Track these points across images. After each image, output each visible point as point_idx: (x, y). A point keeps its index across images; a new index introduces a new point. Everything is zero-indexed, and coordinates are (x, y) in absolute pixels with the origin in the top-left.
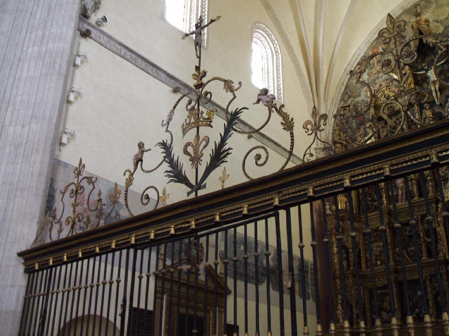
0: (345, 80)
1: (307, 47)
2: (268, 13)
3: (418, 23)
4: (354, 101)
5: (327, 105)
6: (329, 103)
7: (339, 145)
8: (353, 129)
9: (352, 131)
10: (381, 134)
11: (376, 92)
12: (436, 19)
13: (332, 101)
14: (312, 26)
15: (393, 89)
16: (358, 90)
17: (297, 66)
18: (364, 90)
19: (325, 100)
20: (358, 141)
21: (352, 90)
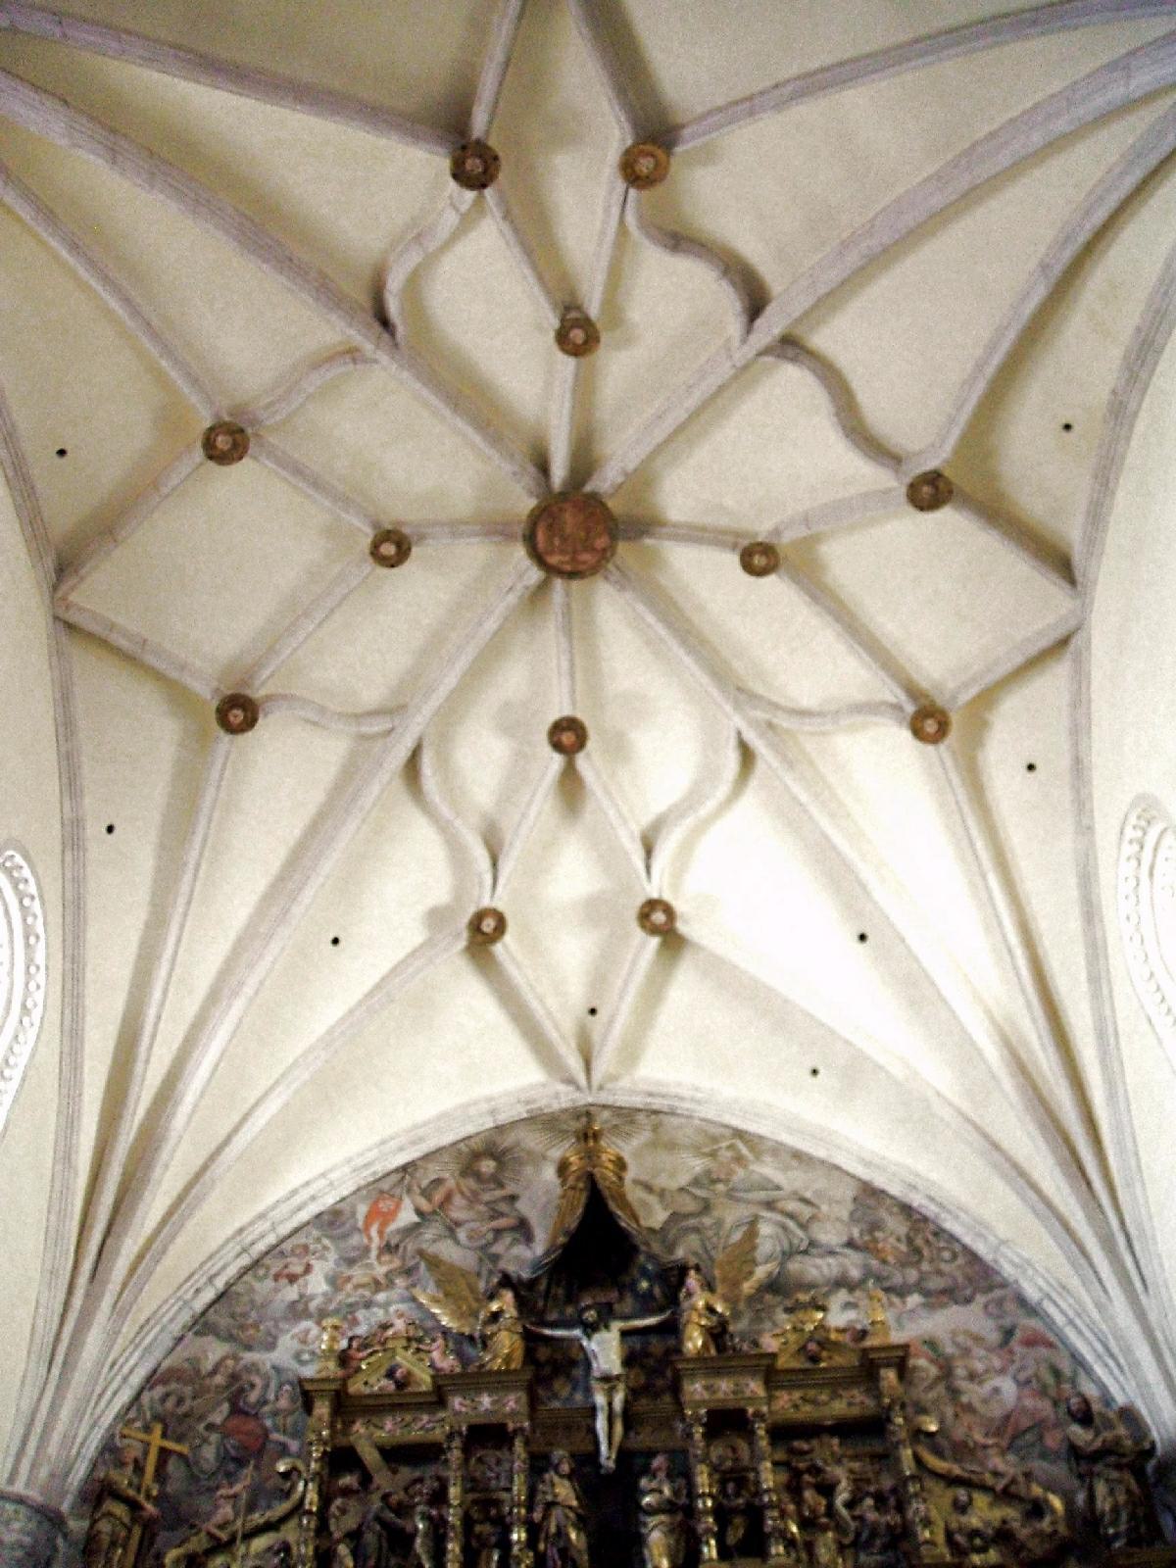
0: (224, 1268)
1: (139, 1068)
2: (63, 861)
3: (589, 1157)
4: (236, 1358)
5: (117, 1333)
6: (128, 1329)
7: (119, 1510)
8: (195, 1470)
9: (193, 1478)
10: (332, 1521)
11: (355, 1344)
12: (644, 1177)
13: (142, 1327)
14: (191, 1008)
15: (436, 1355)
16: (270, 1324)
17: (69, 1122)
18: (296, 1330)
19: (120, 1311)
20: (218, 1518)
21: (244, 1315)
